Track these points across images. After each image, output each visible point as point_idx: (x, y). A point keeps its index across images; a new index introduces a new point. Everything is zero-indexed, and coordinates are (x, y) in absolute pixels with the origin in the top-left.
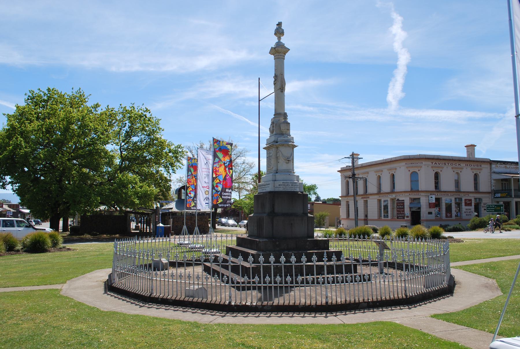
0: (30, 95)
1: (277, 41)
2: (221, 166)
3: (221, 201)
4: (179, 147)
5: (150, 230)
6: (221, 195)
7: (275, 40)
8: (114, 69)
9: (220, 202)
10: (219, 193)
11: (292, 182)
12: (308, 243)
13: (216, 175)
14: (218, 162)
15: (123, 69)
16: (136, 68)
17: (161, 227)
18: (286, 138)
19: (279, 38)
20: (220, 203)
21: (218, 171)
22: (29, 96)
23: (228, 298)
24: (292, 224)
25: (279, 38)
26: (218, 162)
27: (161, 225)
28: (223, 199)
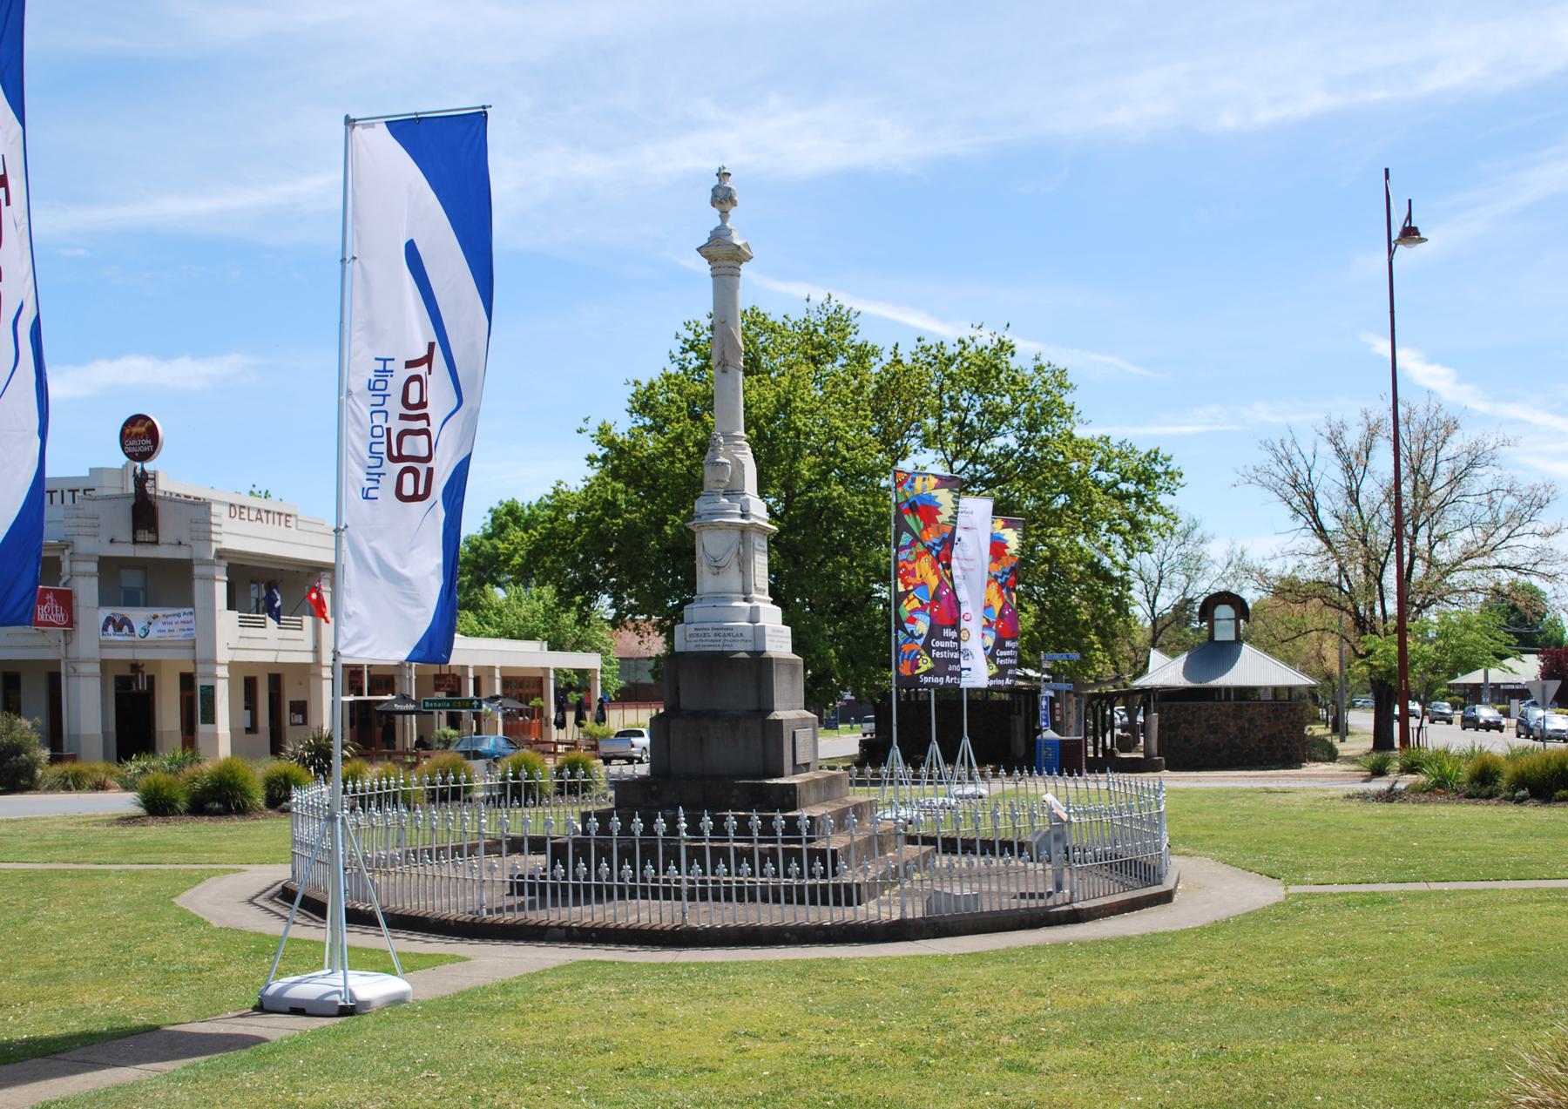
0: (691, 336)
1: (718, 222)
2: (919, 556)
3: (930, 665)
4: (1153, 456)
5: (1096, 752)
6: (927, 647)
7: (712, 218)
8: (1229, 120)
9: (924, 668)
10: (920, 642)
11: (716, 625)
12: (736, 792)
13: (906, 584)
14: (912, 544)
15: (1263, 117)
16: (1313, 101)
17: (1050, 742)
18: (711, 506)
19: (724, 215)
20: (928, 673)
21: (913, 573)
22: (686, 341)
23: (679, 914)
24: (701, 740)
25: (724, 215)
26: (912, 544)
27: (1049, 734)
28: (934, 660)
